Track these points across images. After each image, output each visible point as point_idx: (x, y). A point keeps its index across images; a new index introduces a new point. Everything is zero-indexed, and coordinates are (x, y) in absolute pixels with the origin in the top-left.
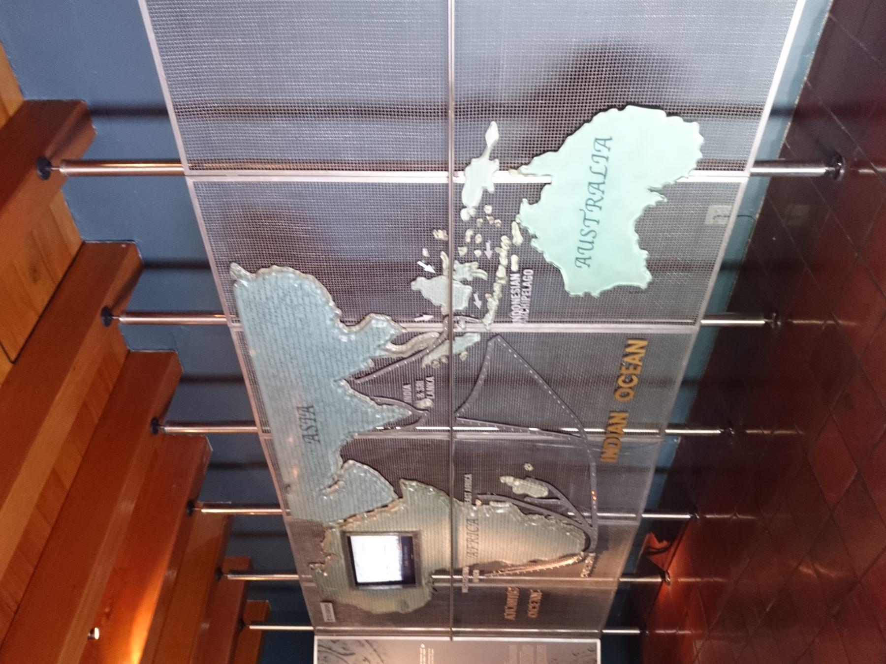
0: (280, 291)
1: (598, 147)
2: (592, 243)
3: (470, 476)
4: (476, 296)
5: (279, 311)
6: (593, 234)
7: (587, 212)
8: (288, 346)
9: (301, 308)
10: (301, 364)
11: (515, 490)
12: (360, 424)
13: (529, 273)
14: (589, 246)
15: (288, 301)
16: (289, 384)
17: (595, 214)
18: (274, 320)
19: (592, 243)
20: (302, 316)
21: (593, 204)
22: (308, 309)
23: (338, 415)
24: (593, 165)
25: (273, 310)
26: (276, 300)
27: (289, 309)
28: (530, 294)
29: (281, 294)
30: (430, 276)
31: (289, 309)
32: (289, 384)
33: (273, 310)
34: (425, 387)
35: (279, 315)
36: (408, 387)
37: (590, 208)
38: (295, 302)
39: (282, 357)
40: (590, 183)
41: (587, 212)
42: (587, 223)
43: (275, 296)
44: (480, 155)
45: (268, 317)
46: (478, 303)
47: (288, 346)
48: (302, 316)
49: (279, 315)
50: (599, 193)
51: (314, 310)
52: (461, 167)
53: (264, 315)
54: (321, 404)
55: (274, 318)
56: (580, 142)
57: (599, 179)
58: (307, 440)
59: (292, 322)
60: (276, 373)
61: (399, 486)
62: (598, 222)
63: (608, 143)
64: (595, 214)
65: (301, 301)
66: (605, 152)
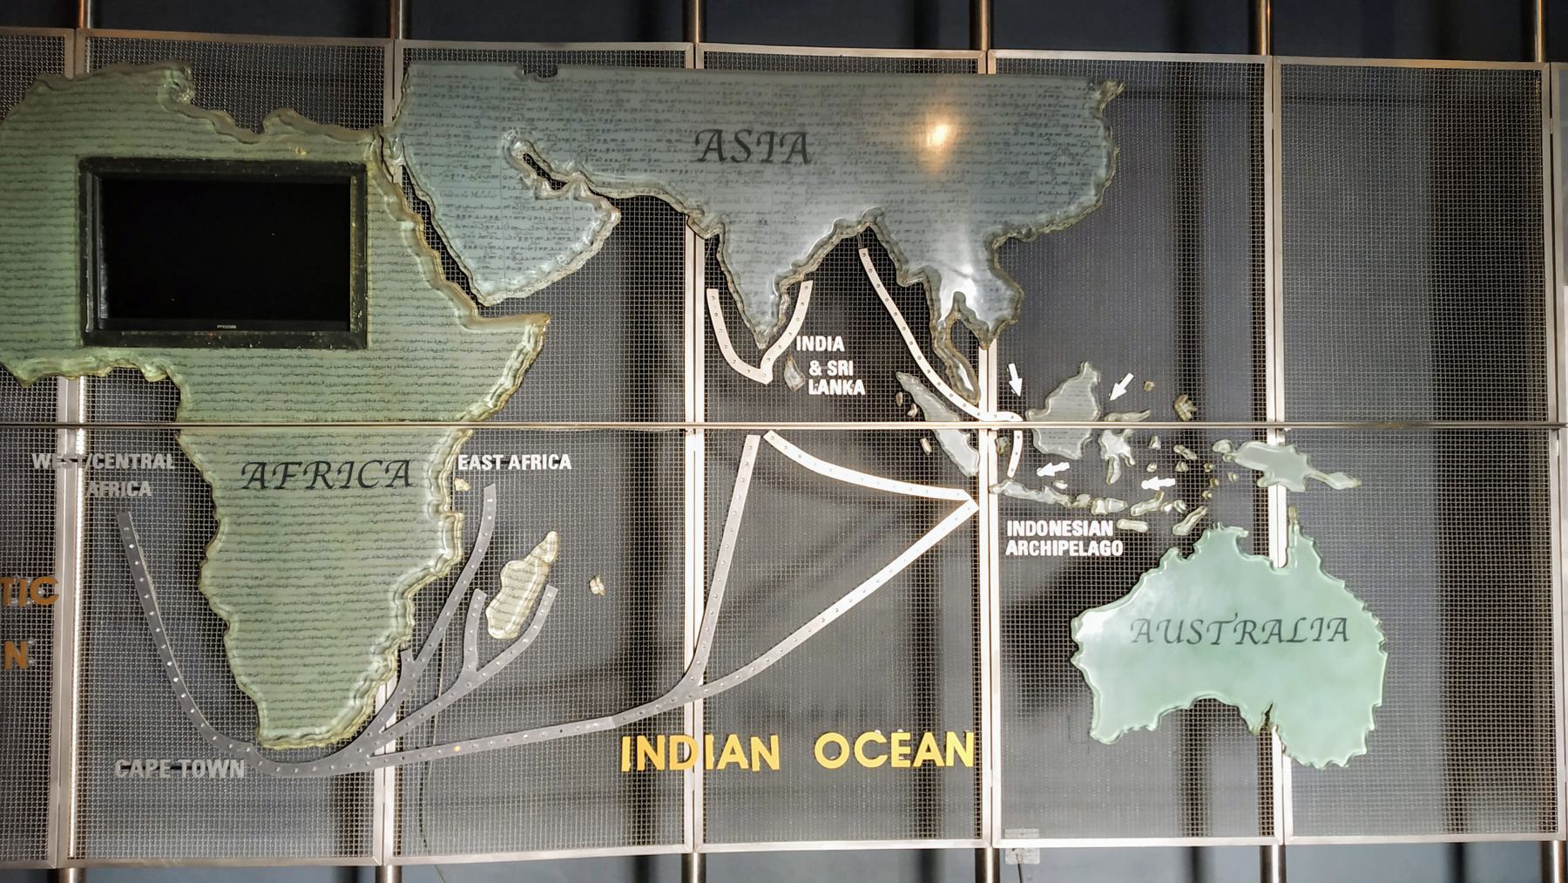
0: (1081, 151)
1: (1334, 624)
2: (1179, 640)
3: (566, 462)
4: (1064, 466)
5: (1041, 140)
6: (1194, 637)
7: (1232, 626)
8: (426, 134)
9: (1049, 178)
10: (654, 156)
11: (514, 565)
12: (751, 247)
13: (1117, 548)
14: (1172, 635)
15: (1063, 159)
16: (601, 126)
17: (1229, 636)
18: (1022, 129)
19: (1179, 640)
20: (1032, 177)
21: (1248, 631)
22: (1047, 188)
23: (511, 202)
24: (1308, 623)
25: (1043, 130)
26: (1062, 140)
27: (1047, 159)
28: (1072, 554)
29: (1074, 150)
30: (1102, 391)
31: (1047, 159)
32: (601, 126)
33: (1043, 130)
34: (837, 377)
35: (1034, 140)
36: (839, 344)
37: (1240, 628)
38: (1058, 170)
39: (668, 126)
40: (1279, 621)
41: (1232, 626)
42: (1214, 628)
43: (1071, 140)
44: (1313, 463)
45: (1031, 120)
46: (1049, 470)
47: (426, 134)
48: (1032, 177)
49: (1034, 140)
50: (1264, 636)
51: (1042, 198)
52: (1296, 439)
53: (768, 113)
54: (1076, 180)
55: (1029, 129)
56: (1339, 598)
57: (1287, 633)
58: (706, 137)
59: (1020, 158)
60: (628, 106)
61: (536, 311)
62: (1216, 643)
63: (1339, 637)
64: (1229, 636)
65: (1061, 179)
66: (1327, 634)
